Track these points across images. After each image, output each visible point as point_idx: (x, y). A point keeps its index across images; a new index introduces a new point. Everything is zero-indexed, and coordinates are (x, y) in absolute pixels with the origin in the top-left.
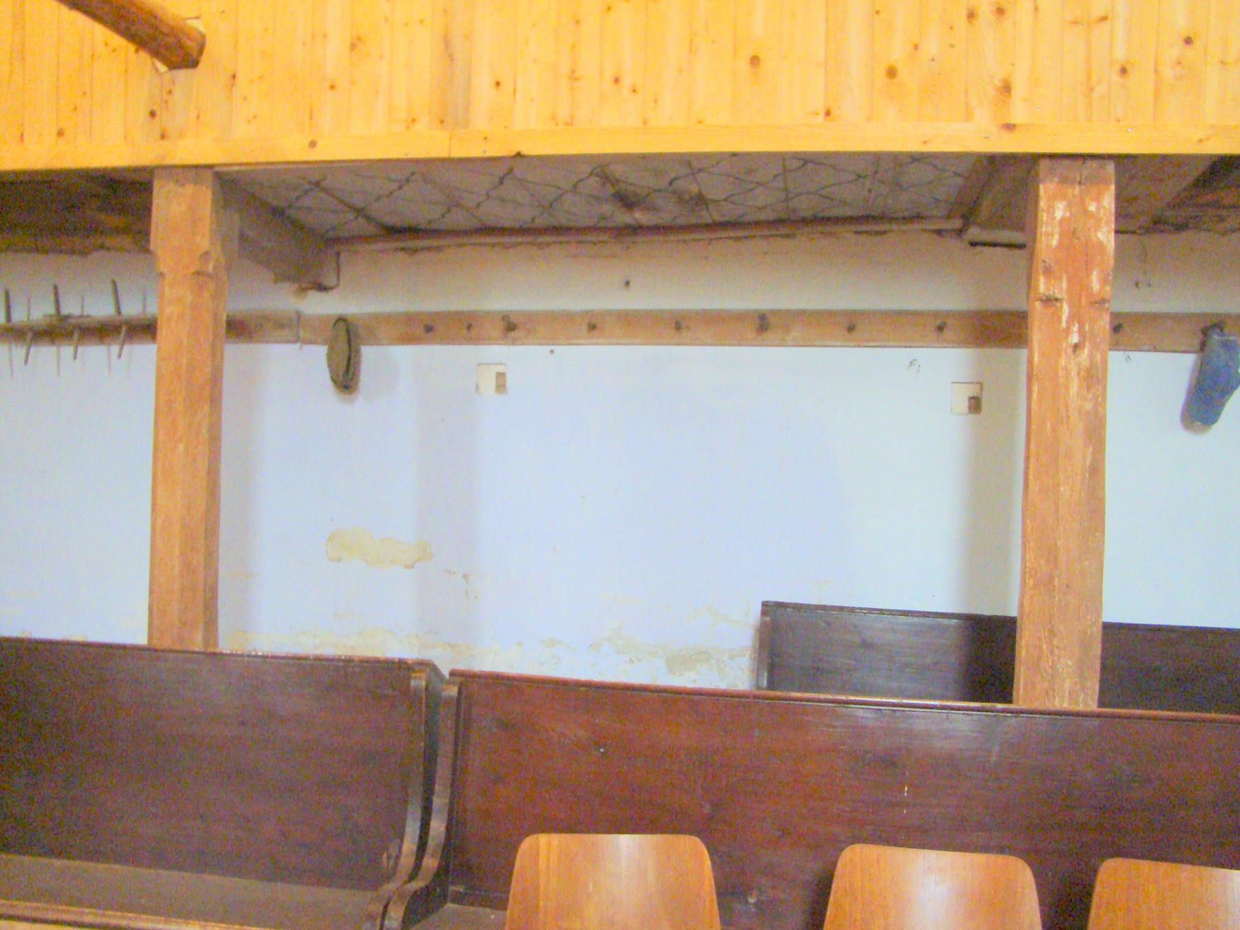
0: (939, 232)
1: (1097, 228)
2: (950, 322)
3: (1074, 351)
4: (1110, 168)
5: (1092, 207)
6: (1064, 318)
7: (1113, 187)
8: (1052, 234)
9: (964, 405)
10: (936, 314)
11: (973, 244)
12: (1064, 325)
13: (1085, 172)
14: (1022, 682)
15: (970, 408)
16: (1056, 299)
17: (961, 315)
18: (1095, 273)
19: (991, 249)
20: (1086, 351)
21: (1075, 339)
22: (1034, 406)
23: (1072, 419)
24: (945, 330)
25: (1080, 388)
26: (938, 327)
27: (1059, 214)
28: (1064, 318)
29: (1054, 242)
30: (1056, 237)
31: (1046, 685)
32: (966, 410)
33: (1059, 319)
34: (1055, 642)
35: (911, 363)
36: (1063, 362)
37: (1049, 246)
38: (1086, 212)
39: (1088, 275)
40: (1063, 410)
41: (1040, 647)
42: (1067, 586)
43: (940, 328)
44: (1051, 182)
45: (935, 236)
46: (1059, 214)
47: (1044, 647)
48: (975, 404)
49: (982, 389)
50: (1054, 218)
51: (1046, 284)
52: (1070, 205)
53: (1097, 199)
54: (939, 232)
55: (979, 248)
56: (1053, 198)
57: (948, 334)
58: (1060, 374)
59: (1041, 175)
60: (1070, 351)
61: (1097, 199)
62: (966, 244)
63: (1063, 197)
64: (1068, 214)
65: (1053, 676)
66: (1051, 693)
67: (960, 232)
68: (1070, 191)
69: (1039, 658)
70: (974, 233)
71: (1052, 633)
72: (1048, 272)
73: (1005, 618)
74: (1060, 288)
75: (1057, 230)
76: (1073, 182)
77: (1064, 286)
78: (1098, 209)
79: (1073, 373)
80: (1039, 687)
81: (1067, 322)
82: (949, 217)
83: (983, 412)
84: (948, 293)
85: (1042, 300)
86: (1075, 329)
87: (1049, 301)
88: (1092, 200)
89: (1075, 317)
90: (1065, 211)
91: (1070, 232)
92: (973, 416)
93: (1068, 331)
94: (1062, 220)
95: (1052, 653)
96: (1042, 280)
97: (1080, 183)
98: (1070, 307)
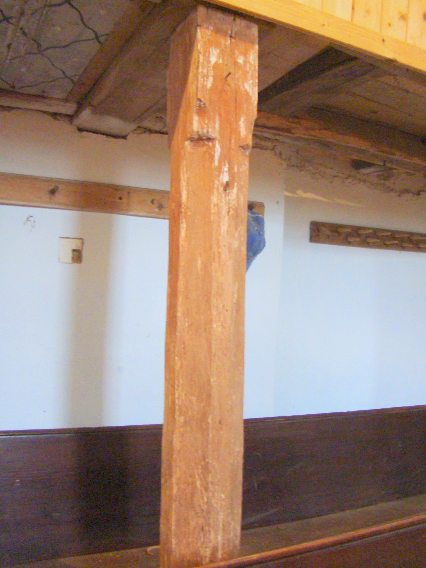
0: (55, 115)
1: (245, 79)
2: (61, 186)
3: (225, 190)
4: (255, 30)
5: (241, 60)
6: (217, 158)
7: (257, 47)
8: (206, 76)
9: (69, 255)
10: (50, 180)
11: (80, 130)
12: (216, 163)
13: (236, 29)
14: (173, 518)
15: (73, 258)
16: (209, 139)
17: (69, 183)
18: (242, 119)
19: (94, 135)
20: (235, 190)
21: (225, 178)
22: (182, 242)
23: (223, 257)
24: (57, 194)
25: (229, 226)
26: (51, 192)
27: (213, 59)
28: (217, 158)
29: (209, 84)
30: (211, 79)
31: (201, 521)
32: (70, 260)
33: (212, 157)
34: (210, 479)
35: (28, 219)
36: (214, 199)
37: (204, 86)
38: (236, 63)
39: (237, 120)
40: (215, 247)
41: (193, 484)
42: (220, 422)
43: (53, 192)
44: (207, 28)
45: (52, 119)
46: (213, 59)
47: (198, 483)
48: (77, 256)
49: (83, 243)
50: (209, 62)
51: (200, 122)
52: (222, 53)
53: (245, 54)
54: (55, 115)
55: (84, 133)
56: (210, 43)
57: (59, 197)
58: (213, 211)
59: (199, 20)
60: (221, 189)
61: (245, 54)
62: (75, 129)
63: (217, 45)
64: (221, 61)
65: (208, 512)
66: (207, 528)
67: (71, 118)
68: (223, 41)
69: (193, 495)
70: (86, 117)
71: (206, 469)
72: (202, 111)
73: (100, 428)
74: (214, 129)
75: (211, 73)
76: (224, 34)
77: (217, 126)
78: (245, 62)
79: (224, 212)
80: (193, 524)
81: (219, 161)
82: (66, 100)
83: (83, 263)
84: (59, 164)
85: (192, 140)
86: (226, 168)
87: (201, 140)
88: (241, 54)
89: (226, 157)
90: (218, 58)
91: (224, 78)
92: (76, 265)
93: (219, 170)
94: (216, 66)
95: (206, 489)
96: (196, 118)
97: (231, 36)
98: (222, 147)
